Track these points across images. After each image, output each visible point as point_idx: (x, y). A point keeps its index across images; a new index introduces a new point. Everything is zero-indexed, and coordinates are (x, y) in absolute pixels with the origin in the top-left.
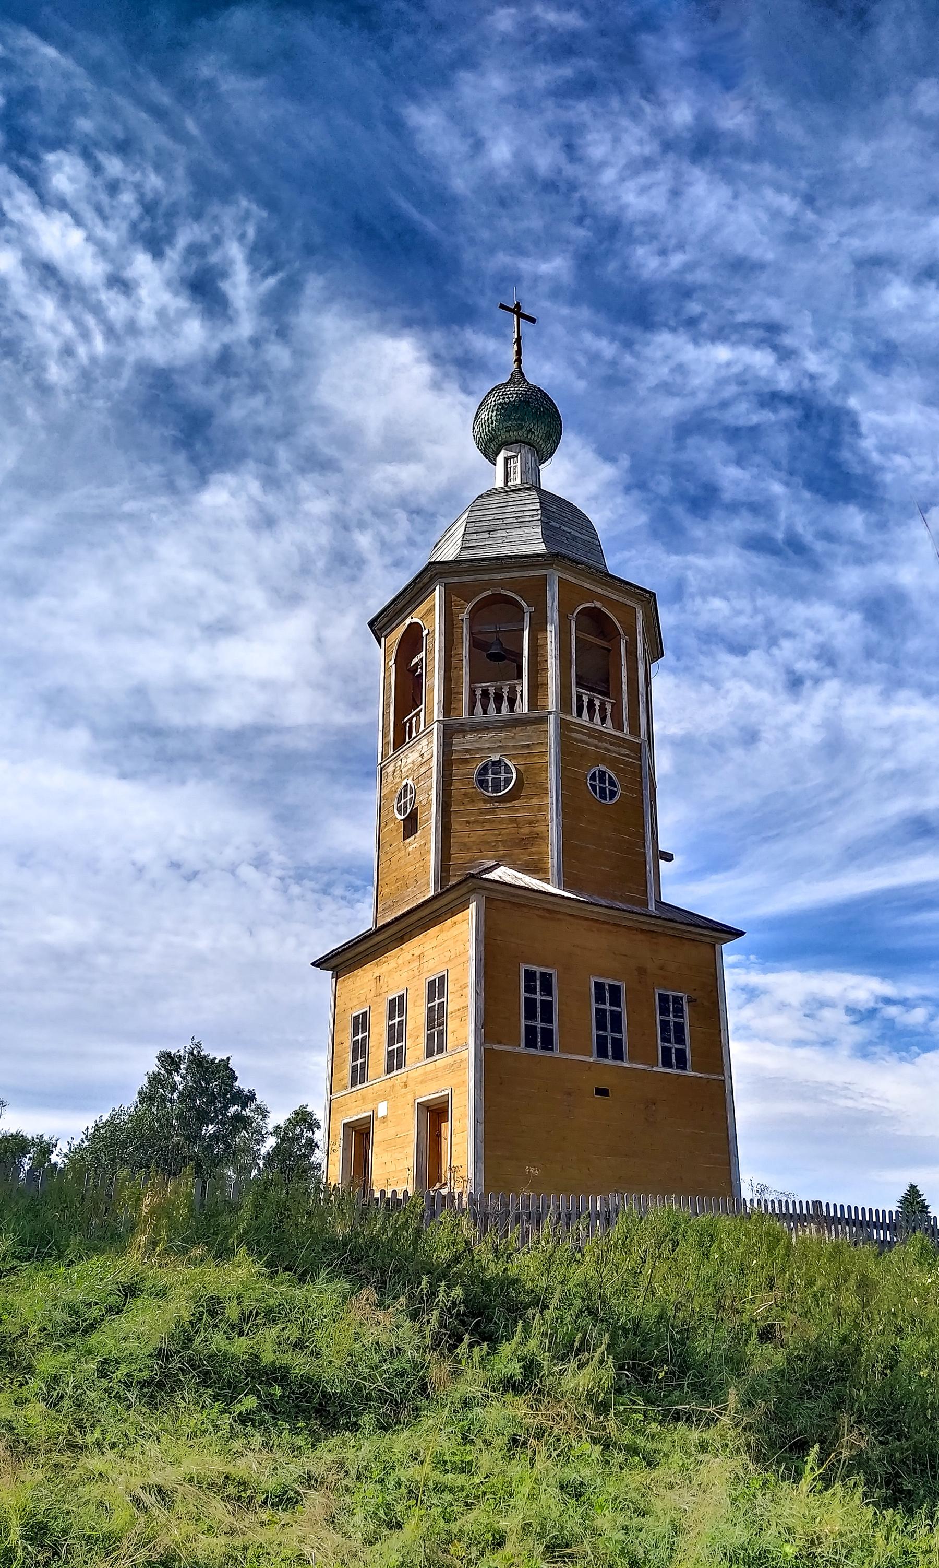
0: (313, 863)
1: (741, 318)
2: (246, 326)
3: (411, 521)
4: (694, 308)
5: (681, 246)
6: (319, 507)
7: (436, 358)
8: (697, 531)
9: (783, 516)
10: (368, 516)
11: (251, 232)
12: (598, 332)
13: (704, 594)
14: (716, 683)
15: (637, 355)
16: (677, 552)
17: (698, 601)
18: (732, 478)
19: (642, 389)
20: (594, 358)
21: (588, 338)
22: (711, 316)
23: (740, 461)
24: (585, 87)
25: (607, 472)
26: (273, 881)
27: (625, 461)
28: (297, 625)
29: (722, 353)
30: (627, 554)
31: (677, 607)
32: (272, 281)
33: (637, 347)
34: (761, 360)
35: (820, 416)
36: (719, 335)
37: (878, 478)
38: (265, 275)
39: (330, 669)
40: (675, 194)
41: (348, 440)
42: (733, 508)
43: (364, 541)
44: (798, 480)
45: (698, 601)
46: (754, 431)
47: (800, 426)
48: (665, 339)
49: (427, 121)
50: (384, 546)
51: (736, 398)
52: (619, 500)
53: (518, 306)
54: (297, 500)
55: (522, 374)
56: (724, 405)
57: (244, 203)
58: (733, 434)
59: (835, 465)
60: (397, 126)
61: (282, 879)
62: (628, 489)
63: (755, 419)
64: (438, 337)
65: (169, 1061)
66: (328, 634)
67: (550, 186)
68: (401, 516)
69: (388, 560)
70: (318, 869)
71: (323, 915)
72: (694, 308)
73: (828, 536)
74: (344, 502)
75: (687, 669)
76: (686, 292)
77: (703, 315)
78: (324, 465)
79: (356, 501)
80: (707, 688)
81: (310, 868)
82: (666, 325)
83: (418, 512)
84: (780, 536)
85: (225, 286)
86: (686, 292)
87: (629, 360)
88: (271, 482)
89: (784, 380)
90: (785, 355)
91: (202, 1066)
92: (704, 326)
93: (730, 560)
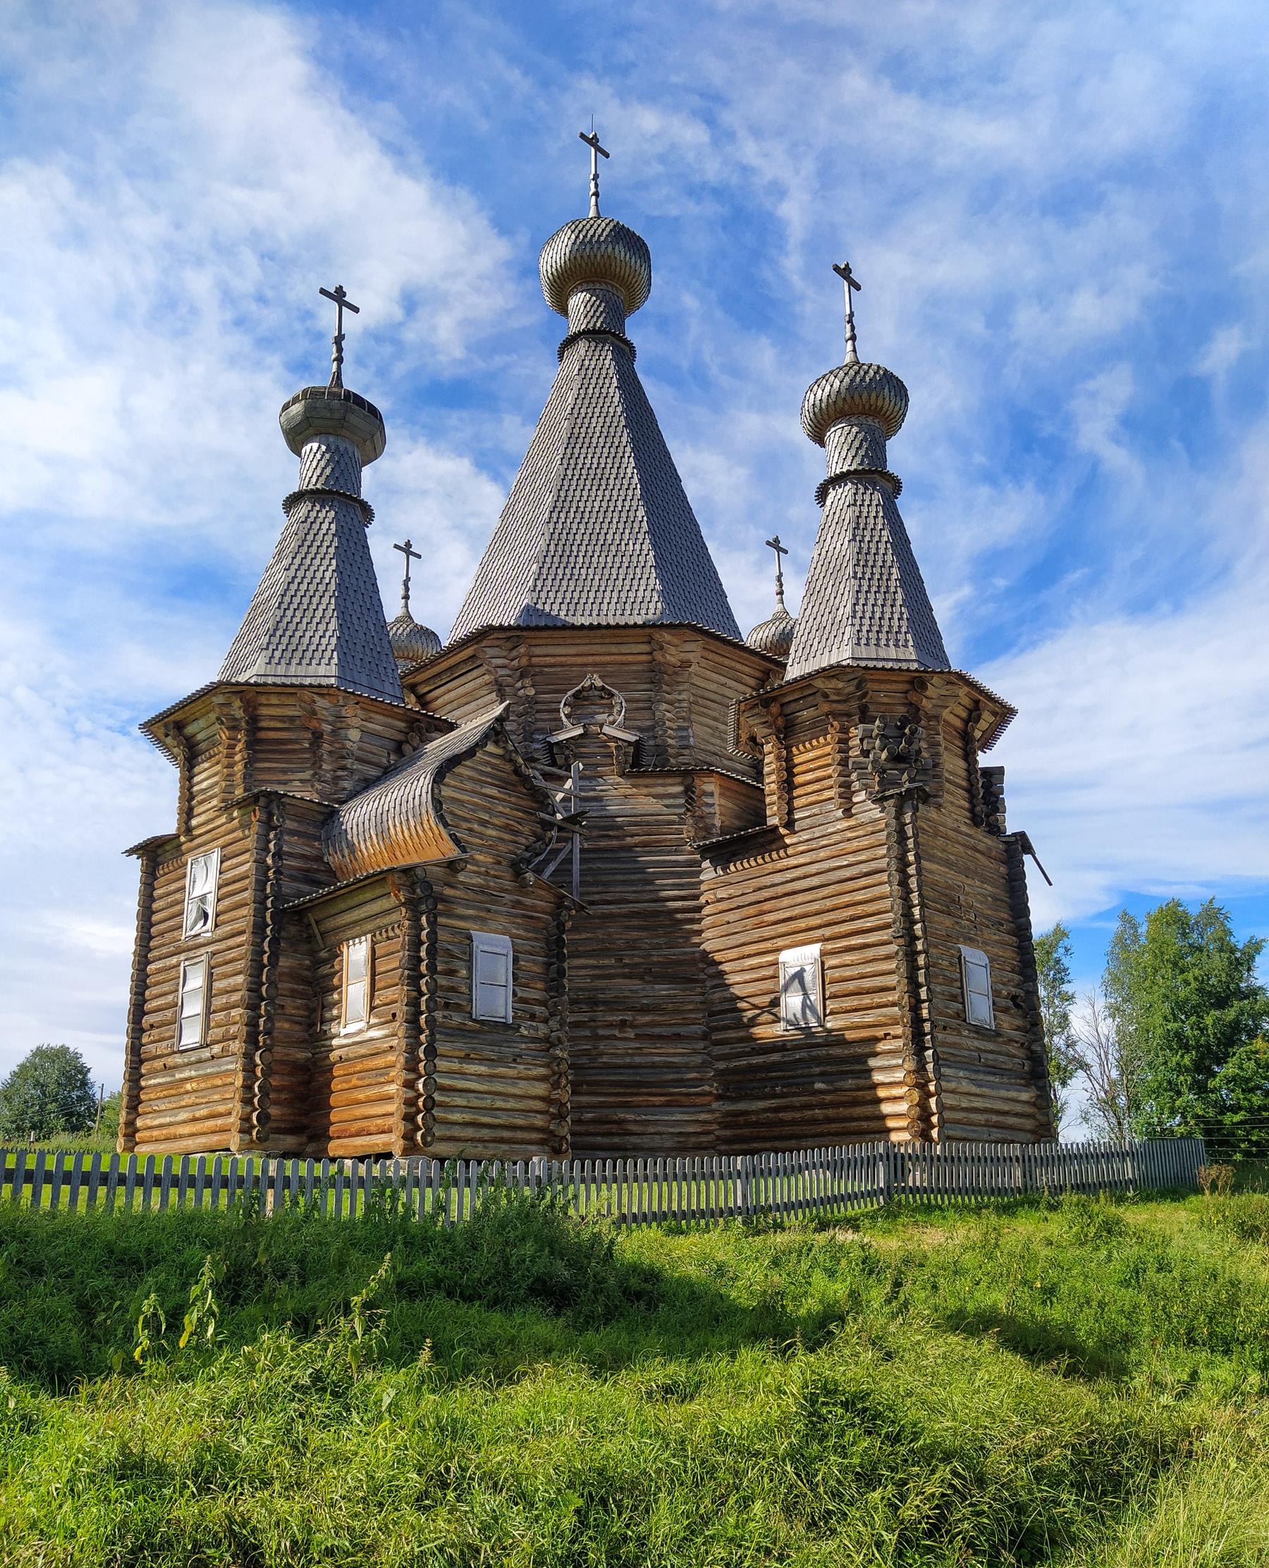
4: (627, 52)
29: (649, 120)
30: (508, 359)
34: (693, 134)
36: (650, 96)
48: (587, 83)
52: (510, 287)
53: (408, 544)
55: (410, 617)
63: (674, 211)
68: (249, 258)
72: (627, 52)
74: (178, 226)
88: (87, 184)
89: (712, 169)
90: (722, 136)
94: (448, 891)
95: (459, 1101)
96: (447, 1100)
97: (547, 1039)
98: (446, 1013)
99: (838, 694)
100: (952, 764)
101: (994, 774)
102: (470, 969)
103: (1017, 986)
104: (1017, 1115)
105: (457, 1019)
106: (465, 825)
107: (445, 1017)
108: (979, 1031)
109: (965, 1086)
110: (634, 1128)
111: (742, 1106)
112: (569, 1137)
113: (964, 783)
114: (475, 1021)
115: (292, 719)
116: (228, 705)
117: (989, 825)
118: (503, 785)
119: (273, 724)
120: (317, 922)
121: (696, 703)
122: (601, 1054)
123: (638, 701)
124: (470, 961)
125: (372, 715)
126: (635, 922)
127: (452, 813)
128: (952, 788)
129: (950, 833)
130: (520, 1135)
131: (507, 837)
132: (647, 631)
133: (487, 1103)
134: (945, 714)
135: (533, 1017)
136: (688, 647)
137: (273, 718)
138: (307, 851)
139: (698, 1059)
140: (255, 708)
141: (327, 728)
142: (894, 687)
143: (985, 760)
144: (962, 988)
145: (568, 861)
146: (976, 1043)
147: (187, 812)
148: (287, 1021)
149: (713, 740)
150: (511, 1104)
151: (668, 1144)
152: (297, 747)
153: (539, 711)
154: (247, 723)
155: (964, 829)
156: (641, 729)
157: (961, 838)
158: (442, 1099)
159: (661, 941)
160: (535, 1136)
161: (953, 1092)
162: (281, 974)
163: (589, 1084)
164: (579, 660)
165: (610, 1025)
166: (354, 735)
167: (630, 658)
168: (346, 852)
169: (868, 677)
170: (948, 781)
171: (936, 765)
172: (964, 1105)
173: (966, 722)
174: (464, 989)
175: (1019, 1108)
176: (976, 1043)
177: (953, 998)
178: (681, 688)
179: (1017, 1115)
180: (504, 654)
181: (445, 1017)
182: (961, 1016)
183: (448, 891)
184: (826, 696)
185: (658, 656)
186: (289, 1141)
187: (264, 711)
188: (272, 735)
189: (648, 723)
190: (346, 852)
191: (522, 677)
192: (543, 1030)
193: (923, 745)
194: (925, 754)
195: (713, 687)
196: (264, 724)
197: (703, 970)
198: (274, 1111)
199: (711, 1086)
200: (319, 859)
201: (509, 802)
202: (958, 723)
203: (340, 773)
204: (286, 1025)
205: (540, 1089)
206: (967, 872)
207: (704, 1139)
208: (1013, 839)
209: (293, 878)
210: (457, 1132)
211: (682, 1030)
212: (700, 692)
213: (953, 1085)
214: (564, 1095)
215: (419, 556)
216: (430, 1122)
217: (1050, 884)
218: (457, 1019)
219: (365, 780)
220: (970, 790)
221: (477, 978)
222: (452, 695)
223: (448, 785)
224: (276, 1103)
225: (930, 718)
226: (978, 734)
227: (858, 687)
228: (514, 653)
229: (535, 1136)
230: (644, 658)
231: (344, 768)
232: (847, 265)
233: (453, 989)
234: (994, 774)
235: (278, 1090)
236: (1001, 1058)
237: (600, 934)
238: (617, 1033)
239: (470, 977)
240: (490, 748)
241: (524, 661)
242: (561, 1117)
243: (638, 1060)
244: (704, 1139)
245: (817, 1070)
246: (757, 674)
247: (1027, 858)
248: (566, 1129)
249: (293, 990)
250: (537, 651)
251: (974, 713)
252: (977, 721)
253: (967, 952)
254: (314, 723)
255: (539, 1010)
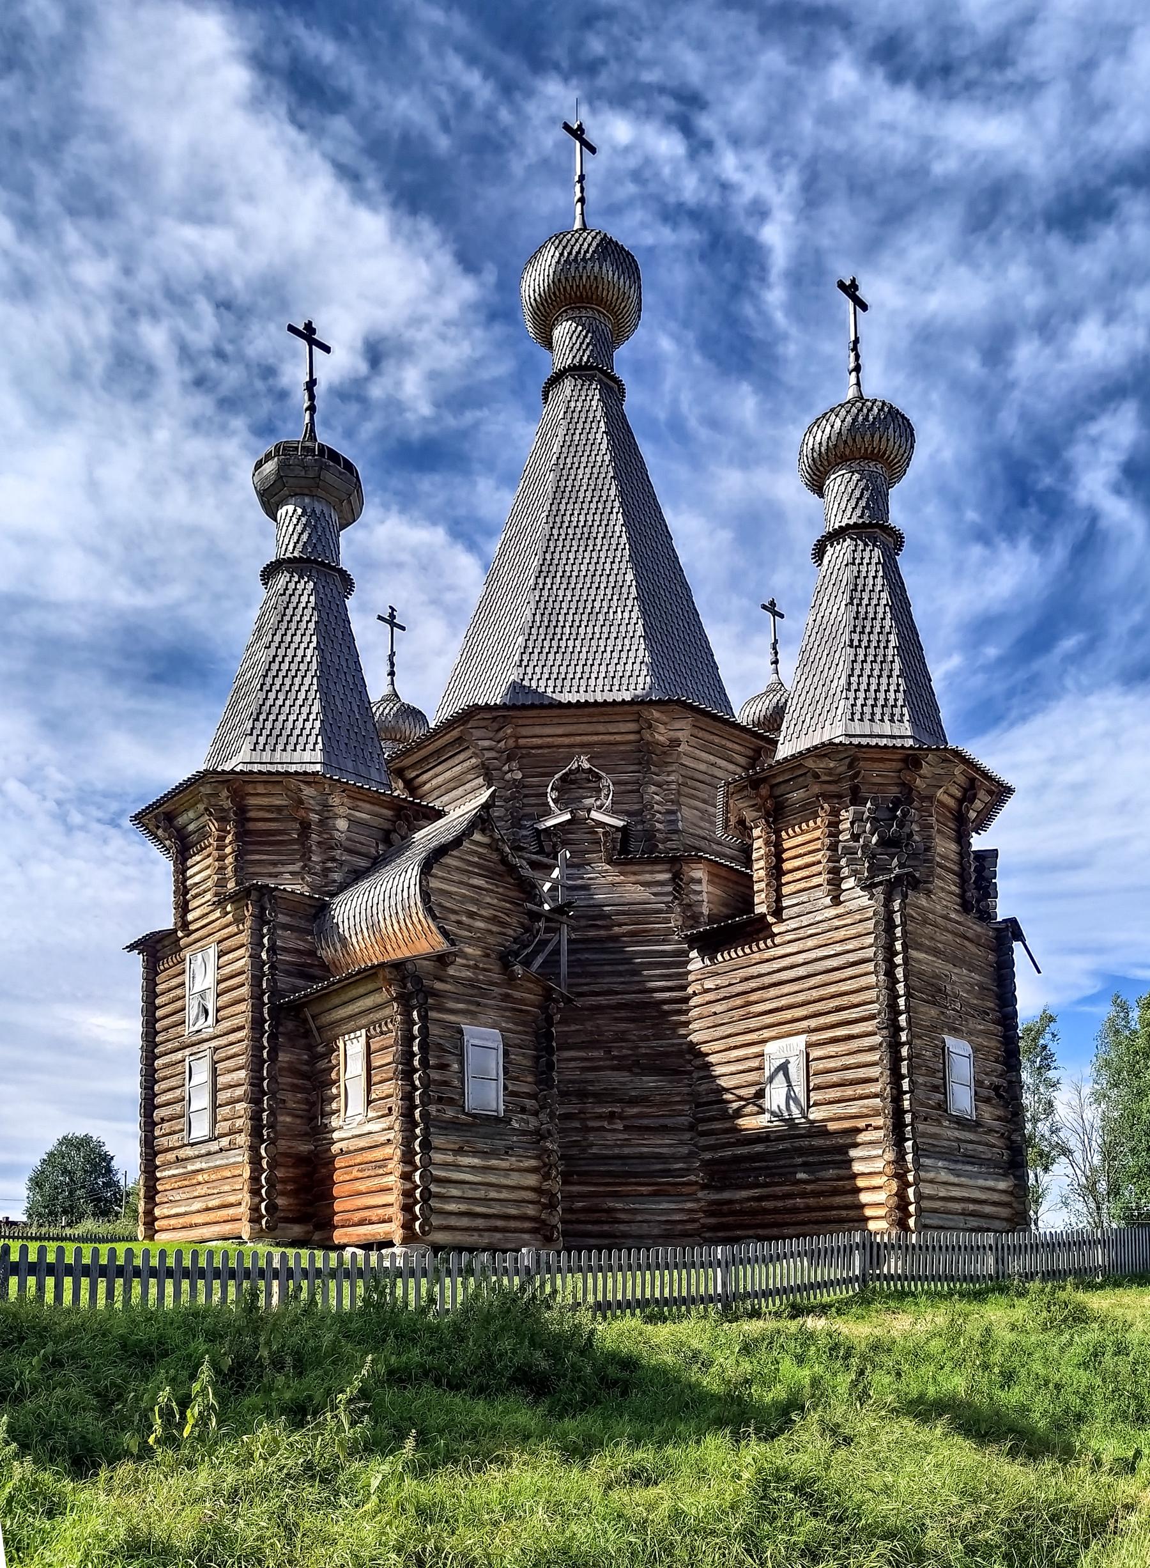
0: (100, 786)
1: (650, 76)
3: (219, 316)
6: (95, 273)
7: (260, 62)
9: (668, 385)
10: (159, 300)
12: (472, 59)
15: (517, 111)
19: (517, 167)
22: (614, 66)
25: (467, 289)
26: (50, 805)
28: (61, 455)
34: (668, 146)
35: (728, 249)
37: (780, 349)
39: (109, 525)
41: (135, 169)
44: (690, 337)
47: (702, 257)
50: (185, 353)
51: (630, 203)
52: (478, 333)
54: (64, 260)
59: (732, 320)
61: (59, 803)
63: (648, 238)
66: (103, 473)
68: (204, 307)
69: (188, 375)
70: (106, 795)
71: (109, 851)
73: (714, 423)
74: (128, 271)
77: (603, 61)
78: (102, 210)
79: (147, 276)
81: (94, 792)
82: (557, 67)
84: (662, 415)
87: (505, 115)
89: (690, 188)
90: (700, 146)
92: (604, 80)
94: (439, 985)
95: (455, 1192)
96: (443, 1191)
97: (537, 1132)
98: (440, 1107)
99: (830, 775)
100: (945, 847)
101: (988, 857)
102: (462, 1064)
103: (1000, 1076)
104: (995, 1204)
105: (450, 1113)
106: (453, 917)
107: (438, 1111)
108: (961, 1122)
109: (944, 1176)
110: (623, 1216)
111: (726, 1195)
112: (560, 1226)
113: (956, 868)
114: (467, 1114)
115: (279, 809)
116: (217, 795)
117: (979, 911)
118: (490, 874)
119: (262, 814)
120: (313, 1017)
121: (685, 785)
122: (591, 1145)
123: (626, 783)
124: (462, 1055)
125: (360, 803)
126: (623, 1014)
127: (440, 905)
128: (943, 873)
129: (939, 920)
130: (513, 1224)
131: (495, 929)
132: (636, 708)
133: (481, 1194)
134: (940, 793)
135: (523, 1110)
136: (677, 725)
137: (261, 808)
138: (302, 945)
139: (685, 1150)
140: (243, 798)
141: (315, 817)
142: (888, 765)
143: (979, 842)
144: (944, 1078)
145: (556, 951)
146: (957, 1134)
147: (183, 908)
148: (288, 1114)
149: (702, 824)
150: (504, 1195)
151: (656, 1231)
152: (286, 838)
153: (526, 796)
154: (235, 814)
155: (953, 916)
156: (628, 814)
157: (949, 925)
158: (438, 1190)
159: (649, 1032)
160: (527, 1225)
161: (931, 1182)
162: (281, 1069)
163: (579, 1174)
164: (566, 741)
165: (600, 1117)
166: (342, 824)
167: (618, 738)
168: (338, 946)
169: (860, 755)
170: (940, 865)
171: (928, 849)
172: (941, 1194)
173: (960, 802)
174: (456, 1083)
175: (996, 1197)
176: (957, 1134)
177: (935, 1089)
178: (670, 769)
179: (995, 1204)
180: (491, 735)
181: (438, 1111)
182: (942, 1106)
183: (439, 985)
184: (816, 776)
185: (646, 735)
186: (297, 1230)
187: (252, 801)
188: (261, 825)
189: (636, 807)
190: (338, 946)
191: (509, 759)
192: (533, 1123)
193: (915, 828)
194: (916, 838)
195: (703, 767)
196: (252, 814)
197: (690, 1061)
198: (281, 1201)
199: (697, 1176)
200: (312, 953)
201: (497, 893)
202: (951, 802)
203: (330, 865)
204: (288, 1119)
205: (532, 1180)
206: (956, 961)
207: (689, 1227)
208: (1003, 926)
209: (289, 973)
210: (453, 1221)
211: (669, 1122)
212: (690, 773)
213: (931, 1175)
214: (555, 1186)
215: (403, 628)
216: (427, 1212)
217: (1039, 972)
218: (450, 1113)
219: (355, 871)
220: (962, 876)
221: (469, 1071)
222: (440, 779)
223: (435, 876)
224: (283, 1193)
225: (923, 799)
226: (973, 815)
227: (851, 766)
228: (501, 734)
229: (527, 1225)
230: (632, 737)
231: (333, 860)
232: (853, 281)
233: (445, 1083)
234: (988, 857)
235: (283, 1181)
236: (981, 1148)
237: (589, 1026)
238: (605, 1124)
239: (462, 1071)
240: (477, 837)
241: (511, 742)
242: (552, 1206)
243: (626, 1151)
244: (689, 1227)
245: (800, 1160)
246: (750, 753)
247: (1017, 946)
248: (557, 1219)
249: (293, 1085)
250: (524, 731)
251: (969, 793)
252: (972, 802)
253: (951, 1041)
254: (302, 813)
255: (529, 1103)
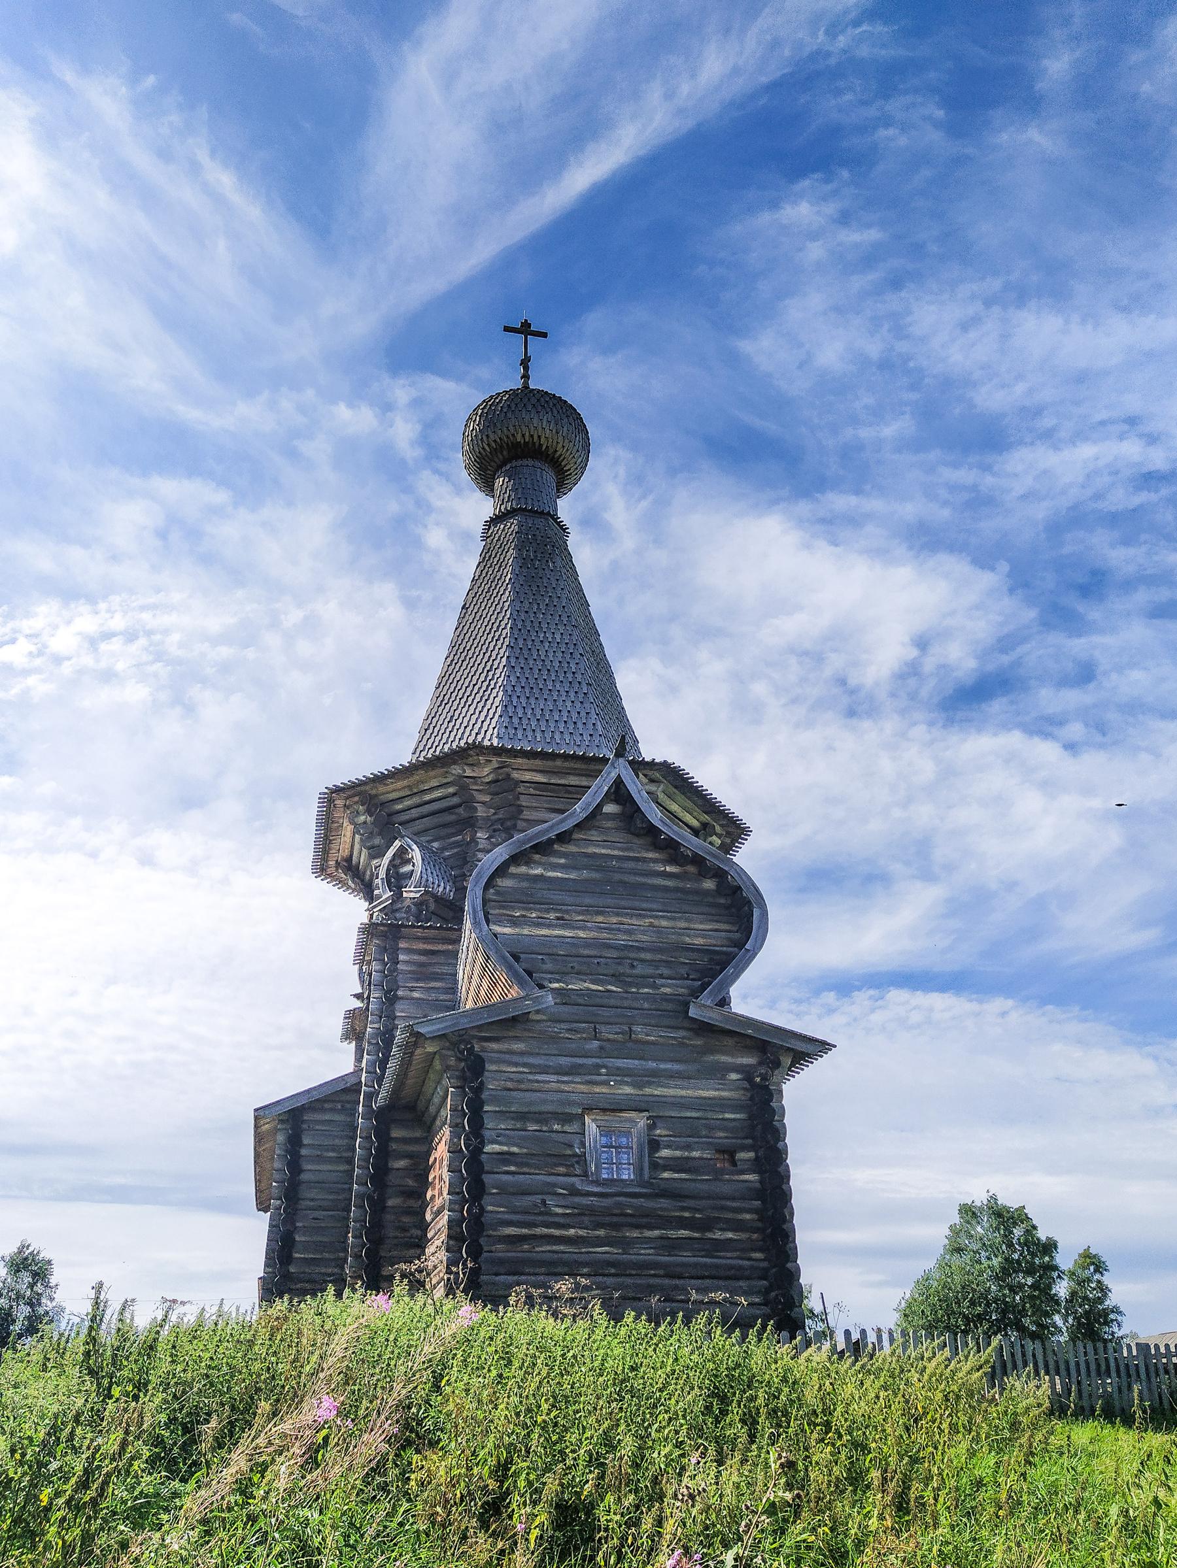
2: (628, 542)
4: (1048, 422)
5: (1020, 377)
8: (1093, 613)
11: (622, 471)
12: (956, 466)
13: (1120, 669)
14: (1156, 754)
16: (1080, 636)
17: (1114, 676)
18: (1121, 558)
20: (953, 488)
21: (949, 475)
23: (1126, 542)
24: (896, 283)
27: (1004, 567)
29: (1087, 451)
31: (1092, 686)
32: (644, 504)
33: (996, 468)
34: (1131, 450)
36: (1079, 436)
38: (639, 500)
40: (1005, 337)
42: (1129, 585)
43: (759, 689)
45: (1114, 676)
46: (1135, 513)
49: (764, 349)
56: (1098, 496)
57: (612, 452)
58: (1113, 519)
60: (734, 359)
62: (1011, 591)
64: (804, 507)
65: (969, 1212)
67: (885, 365)
72: (1048, 422)
75: (1115, 743)
76: (1038, 411)
80: (1144, 756)
82: (1021, 442)
83: (806, 653)
85: (607, 516)
86: (1038, 411)
87: (989, 480)
91: (1006, 1218)
93: (1138, 632)
